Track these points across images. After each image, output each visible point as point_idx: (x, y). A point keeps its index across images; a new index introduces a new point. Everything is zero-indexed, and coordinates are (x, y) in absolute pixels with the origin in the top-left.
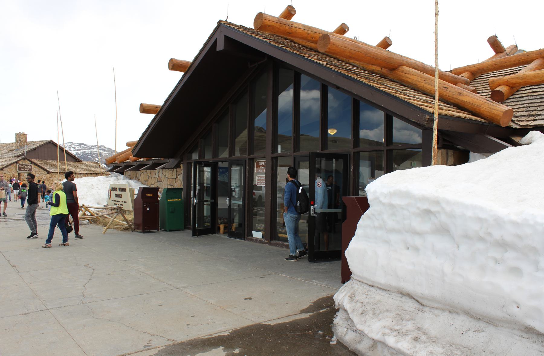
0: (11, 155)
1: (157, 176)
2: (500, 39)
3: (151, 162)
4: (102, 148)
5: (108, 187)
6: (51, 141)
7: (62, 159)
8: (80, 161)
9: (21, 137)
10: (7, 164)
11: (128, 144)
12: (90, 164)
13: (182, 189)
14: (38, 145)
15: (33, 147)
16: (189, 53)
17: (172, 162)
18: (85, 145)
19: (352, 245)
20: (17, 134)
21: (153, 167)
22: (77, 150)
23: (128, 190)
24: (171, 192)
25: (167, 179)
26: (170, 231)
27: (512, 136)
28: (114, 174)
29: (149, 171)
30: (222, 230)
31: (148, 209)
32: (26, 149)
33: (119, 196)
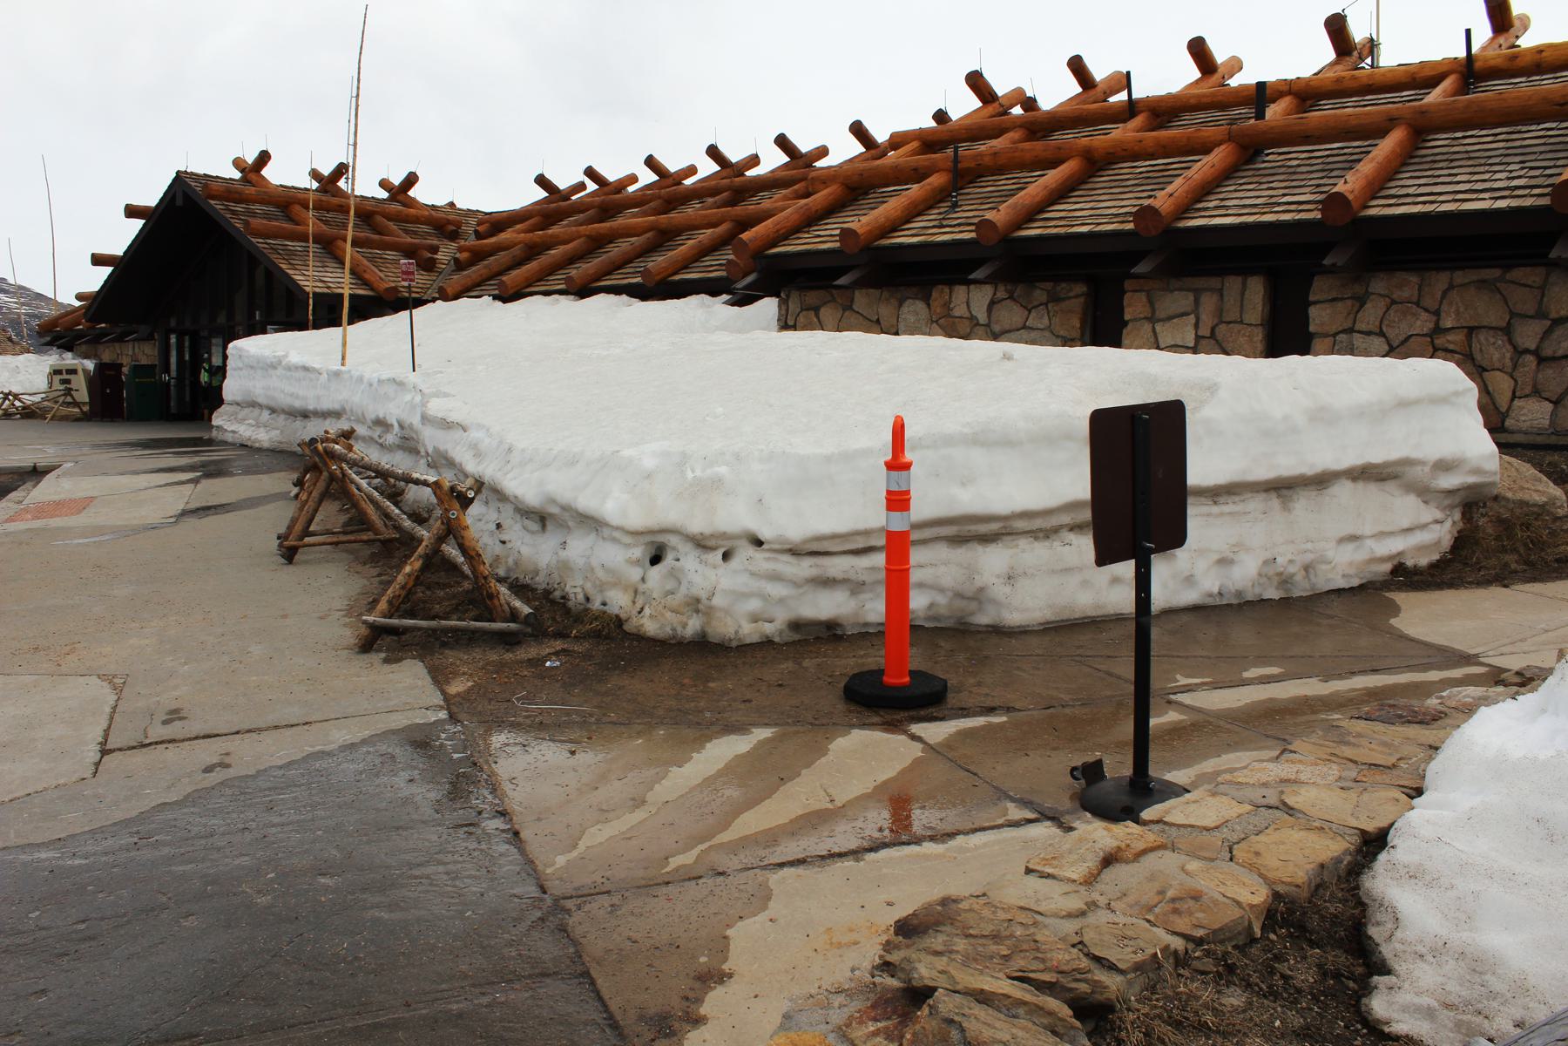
3: (118, 330)
11: (79, 297)
16: (151, 198)
21: (120, 339)
23: (80, 372)
24: (138, 369)
25: (135, 354)
29: (117, 345)
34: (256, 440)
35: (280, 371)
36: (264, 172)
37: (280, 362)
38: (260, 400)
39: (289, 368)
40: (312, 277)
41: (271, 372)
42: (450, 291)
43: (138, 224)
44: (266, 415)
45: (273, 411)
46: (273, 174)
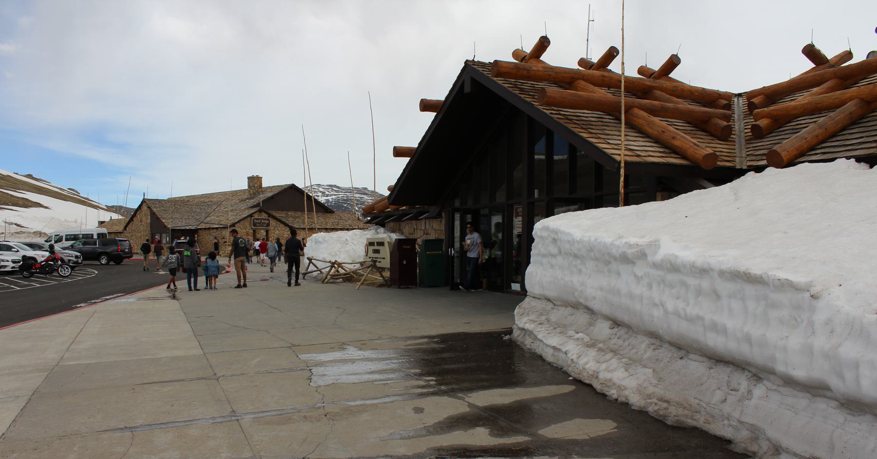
0: (243, 206)
1: (423, 228)
2: (818, 46)
4: (364, 191)
5: (365, 242)
6: (293, 185)
7: (310, 210)
8: (331, 212)
9: (255, 181)
10: (239, 218)
12: (346, 216)
13: (442, 240)
14: (276, 192)
16: (440, 93)
17: (434, 210)
18: (338, 187)
19: (530, 270)
20: (249, 178)
21: (416, 218)
22: (327, 196)
23: (386, 244)
26: (430, 287)
27: (724, 175)
28: (373, 227)
29: (414, 222)
30: (484, 285)
32: (262, 197)
33: (377, 251)
34: (609, 383)
35: (640, 269)
36: (543, 58)
37: (643, 255)
38: (595, 305)
39: (673, 267)
40: (623, 147)
41: (623, 268)
42: (785, 156)
43: (431, 116)
44: (603, 329)
45: (616, 323)
46: (549, 58)
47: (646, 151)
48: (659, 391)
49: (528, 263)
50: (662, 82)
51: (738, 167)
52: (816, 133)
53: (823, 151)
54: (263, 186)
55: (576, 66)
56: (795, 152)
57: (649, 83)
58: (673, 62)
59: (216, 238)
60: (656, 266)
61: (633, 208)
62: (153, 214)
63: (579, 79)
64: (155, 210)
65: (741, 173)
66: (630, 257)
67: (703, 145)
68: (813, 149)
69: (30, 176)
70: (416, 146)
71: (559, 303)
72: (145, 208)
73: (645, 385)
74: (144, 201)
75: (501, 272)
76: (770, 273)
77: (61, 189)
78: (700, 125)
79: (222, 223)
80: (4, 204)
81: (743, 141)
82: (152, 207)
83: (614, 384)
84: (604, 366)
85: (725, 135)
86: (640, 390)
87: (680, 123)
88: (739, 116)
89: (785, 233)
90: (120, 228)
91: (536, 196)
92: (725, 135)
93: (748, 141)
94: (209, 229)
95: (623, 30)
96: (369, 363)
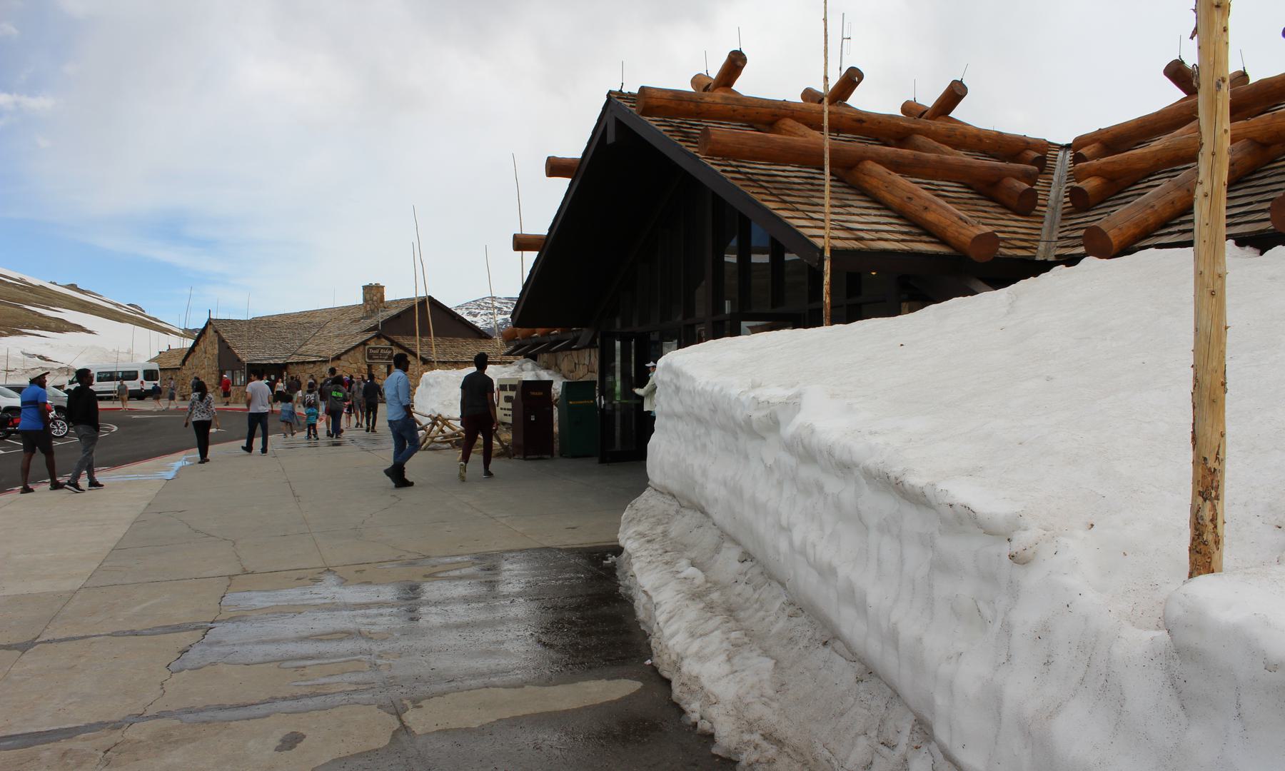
0: (355, 329)
10: (347, 347)
15: (394, 312)
16: (574, 147)
17: (586, 334)
20: (365, 288)
31: (533, 419)
32: (382, 316)
35: (771, 452)
37: (774, 424)
39: (807, 453)
42: (1114, 236)
43: (563, 184)
46: (745, 86)
47: (877, 231)
48: (769, 716)
49: (653, 431)
50: (938, 125)
51: (1040, 258)
52: (1170, 197)
53: (1182, 227)
54: (387, 298)
55: (797, 98)
56: (1133, 231)
57: (906, 124)
58: (955, 94)
59: (312, 376)
60: (789, 447)
61: (838, 327)
62: (222, 341)
63: (785, 116)
64: (224, 335)
65: (1045, 266)
66: (755, 426)
67: (975, 222)
68: (1166, 225)
69: (73, 287)
70: (545, 232)
71: (685, 504)
72: (210, 332)
73: (749, 699)
74: (210, 322)
75: (613, 438)
76: (942, 486)
77: (117, 305)
78: (986, 189)
79: (323, 354)
80: (27, 327)
81: (1059, 216)
82: (221, 330)
83: (702, 688)
84: (695, 646)
85: (1026, 206)
86: (739, 708)
87: (951, 188)
88: (1060, 177)
89: (1049, 379)
90: (176, 362)
91: (728, 309)
92: (1026, 206)
93: (1066, 217)
94: (303, 363)
95: (825, 20)
96: (321, 615)
